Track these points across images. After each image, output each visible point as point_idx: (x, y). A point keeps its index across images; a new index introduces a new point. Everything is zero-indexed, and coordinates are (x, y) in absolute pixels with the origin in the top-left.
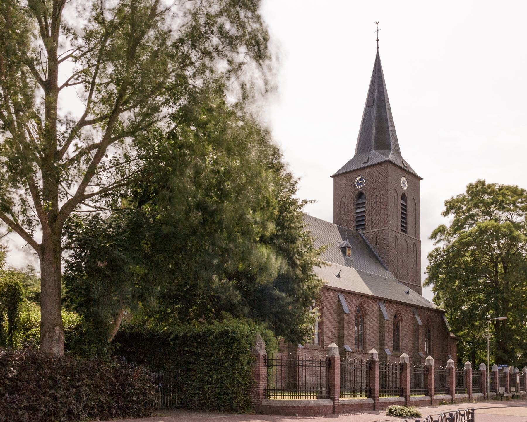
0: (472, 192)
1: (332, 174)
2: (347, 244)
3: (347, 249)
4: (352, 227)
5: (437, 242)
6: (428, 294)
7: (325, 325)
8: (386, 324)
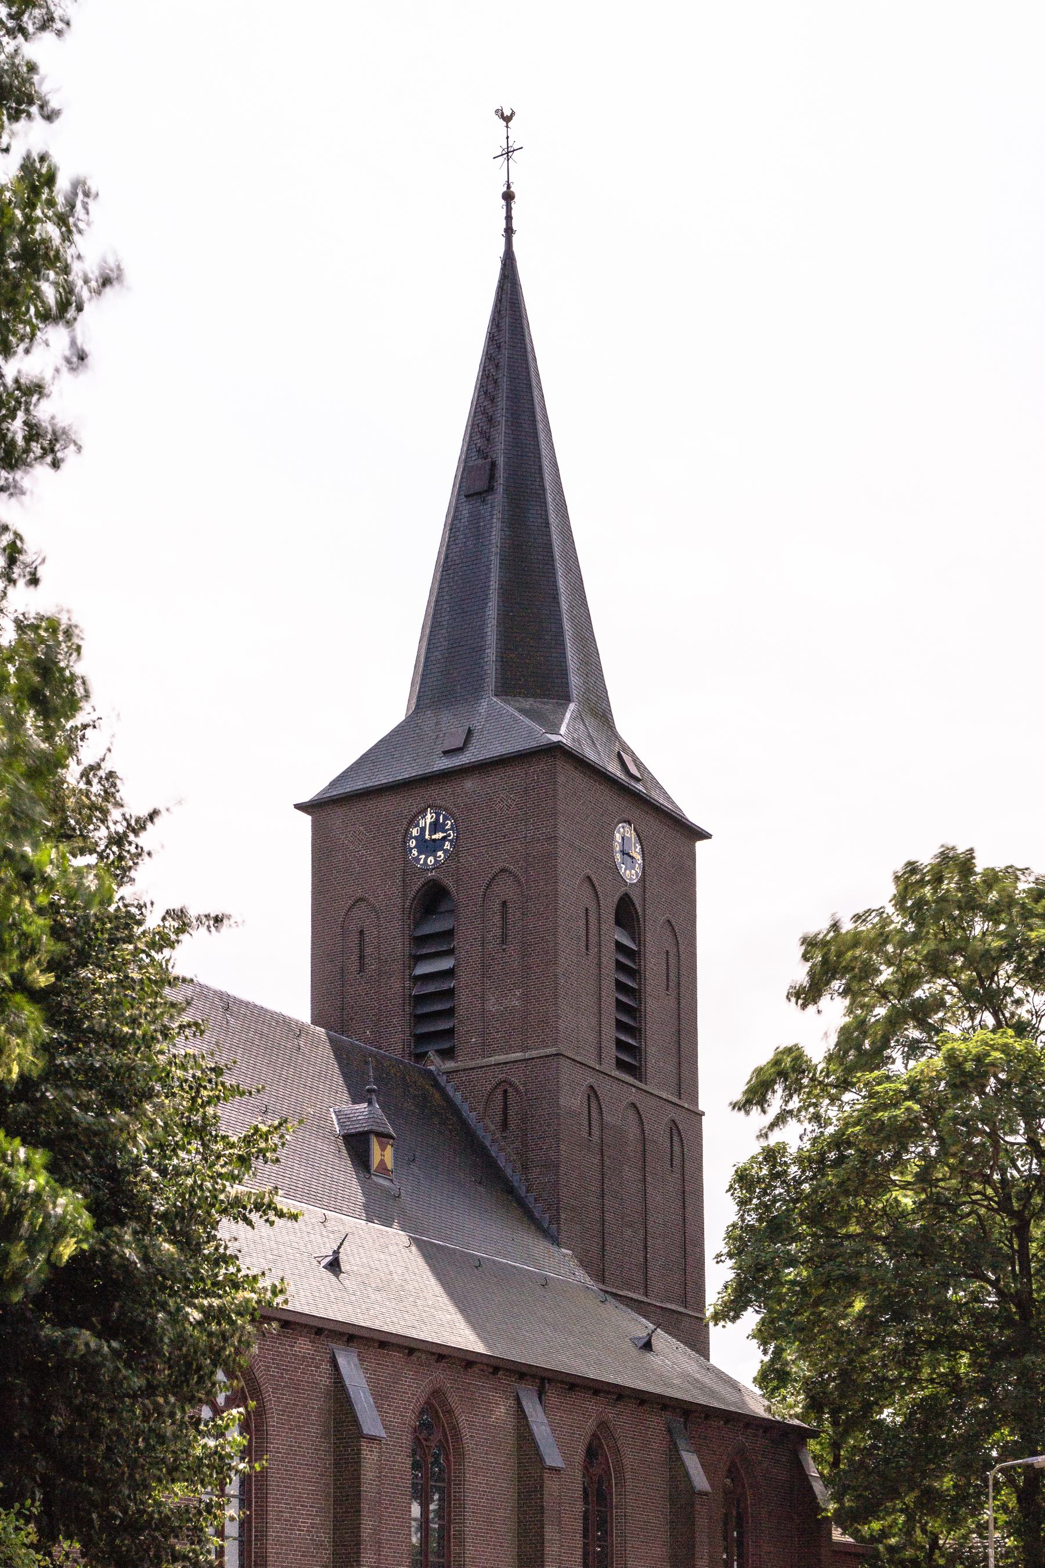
0: (920, 903)
1: (306, 797)
4: (396, 1042)
5: (773, 1126)
6: (736, 1352)
8: (552, 1486)
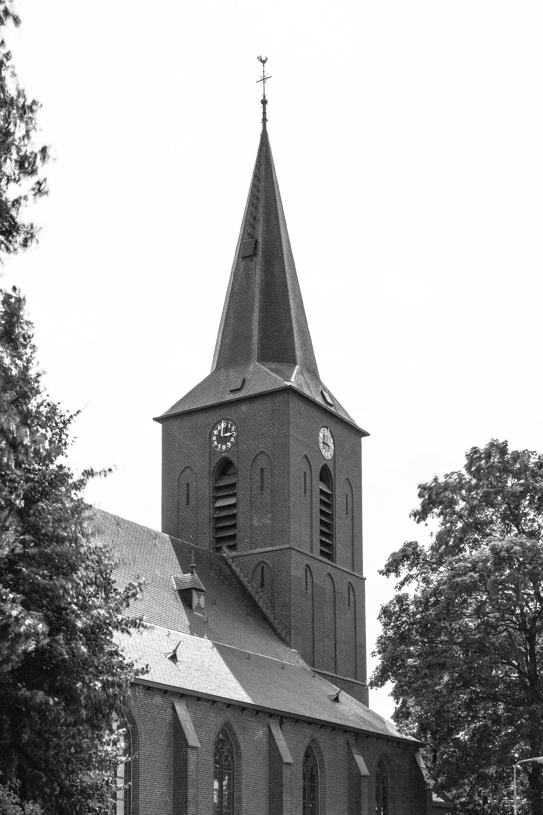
0: (479, 469)
1: (159, 414)
2: (193, 581)
3: (195, 594)
4: (206, 542)
5: (402, 584)
6: (383, 703)
7: (142, 769)
8: (287, 773)
